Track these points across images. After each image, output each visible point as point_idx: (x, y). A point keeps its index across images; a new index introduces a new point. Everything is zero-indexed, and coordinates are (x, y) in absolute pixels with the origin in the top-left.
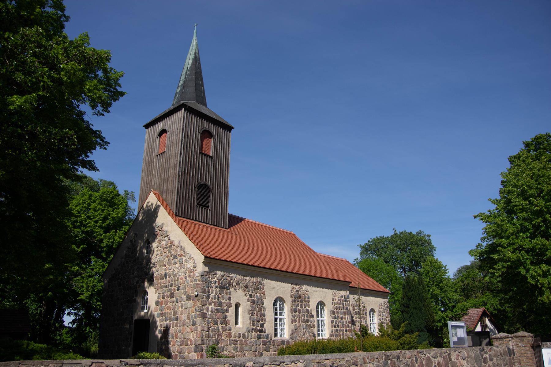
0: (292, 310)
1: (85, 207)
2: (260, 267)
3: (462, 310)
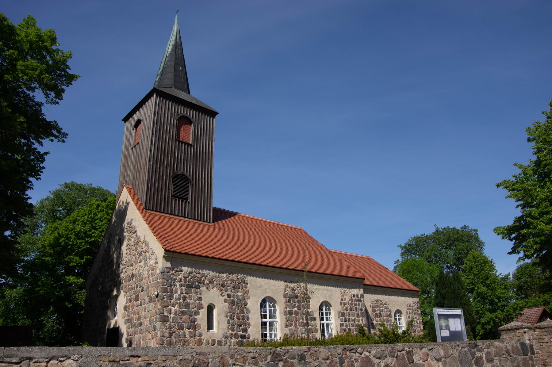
1: (91, 217)
2: (241, 262)
3: (515, 310)
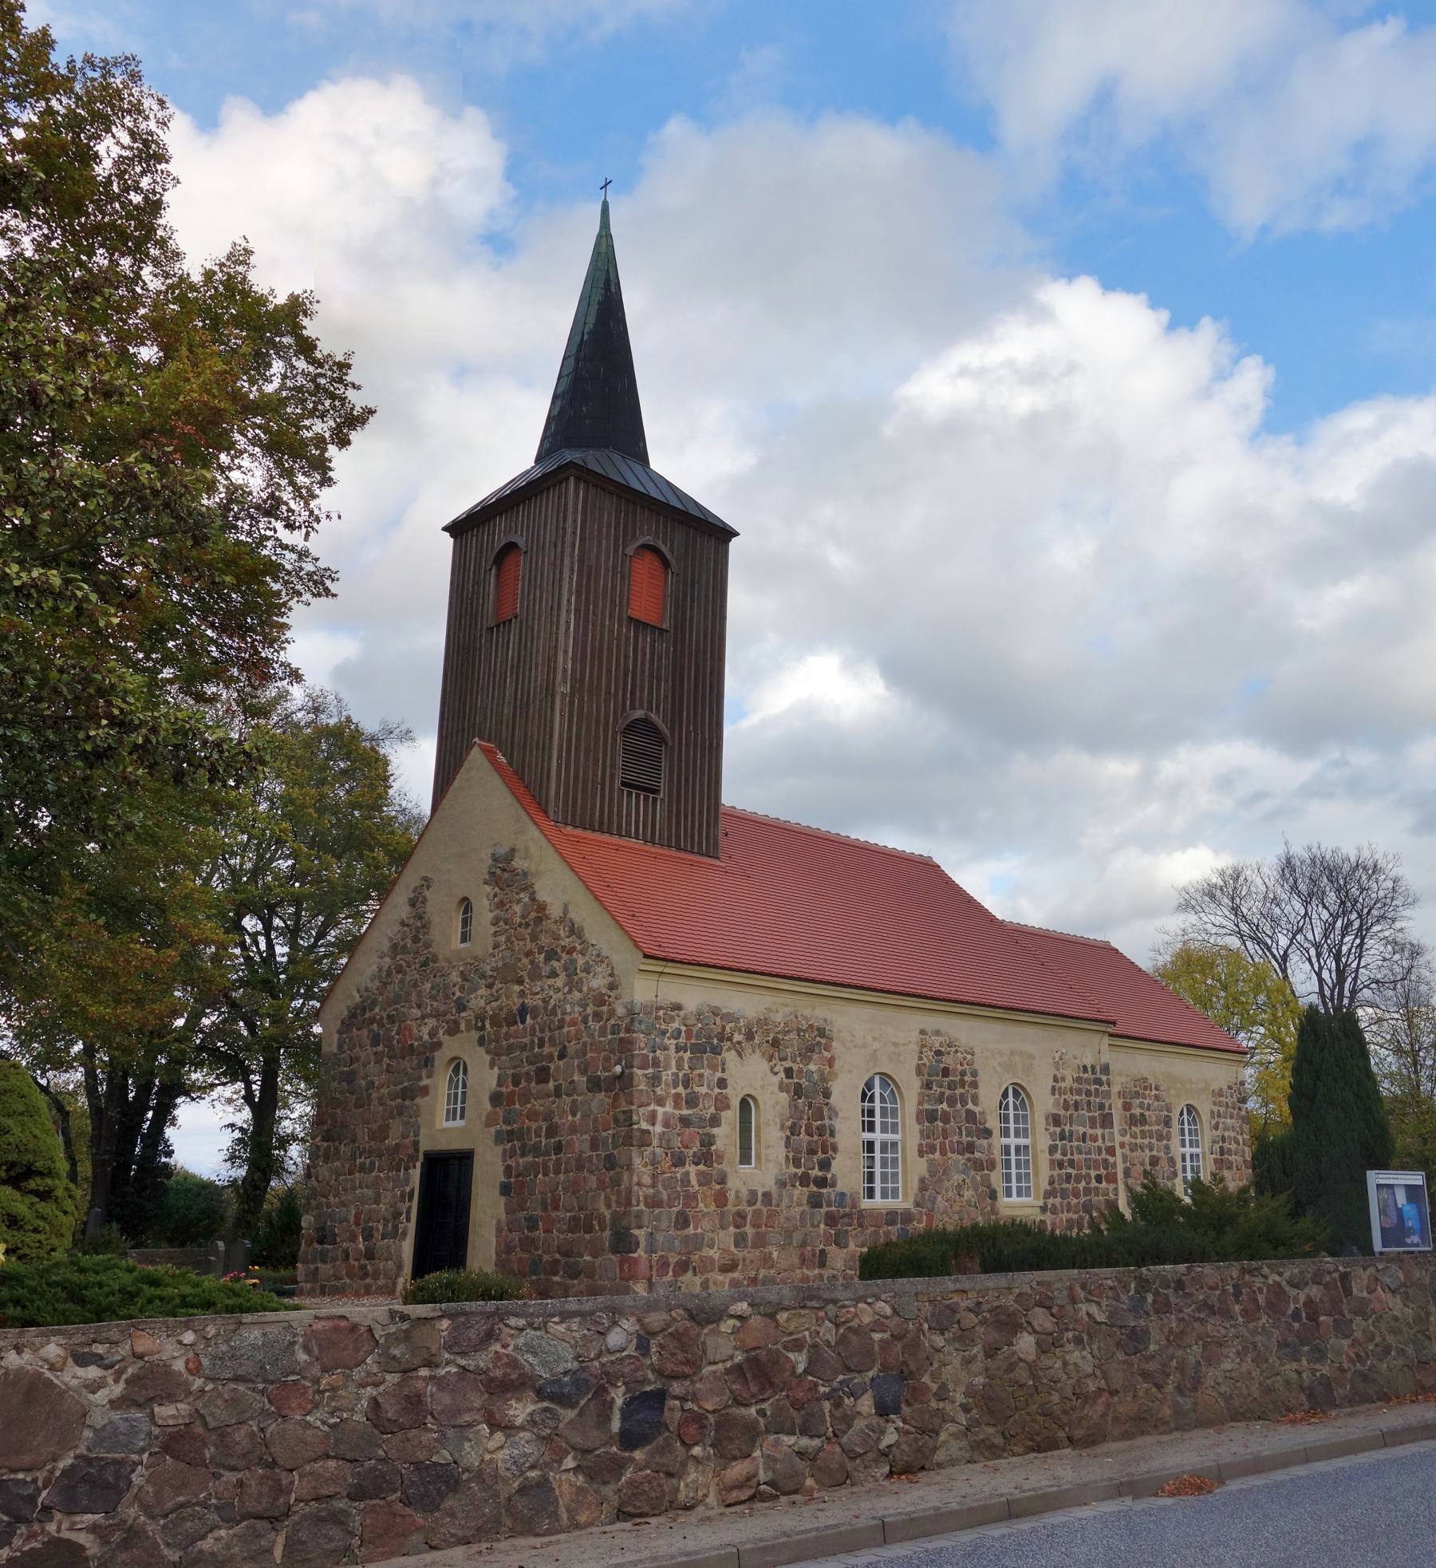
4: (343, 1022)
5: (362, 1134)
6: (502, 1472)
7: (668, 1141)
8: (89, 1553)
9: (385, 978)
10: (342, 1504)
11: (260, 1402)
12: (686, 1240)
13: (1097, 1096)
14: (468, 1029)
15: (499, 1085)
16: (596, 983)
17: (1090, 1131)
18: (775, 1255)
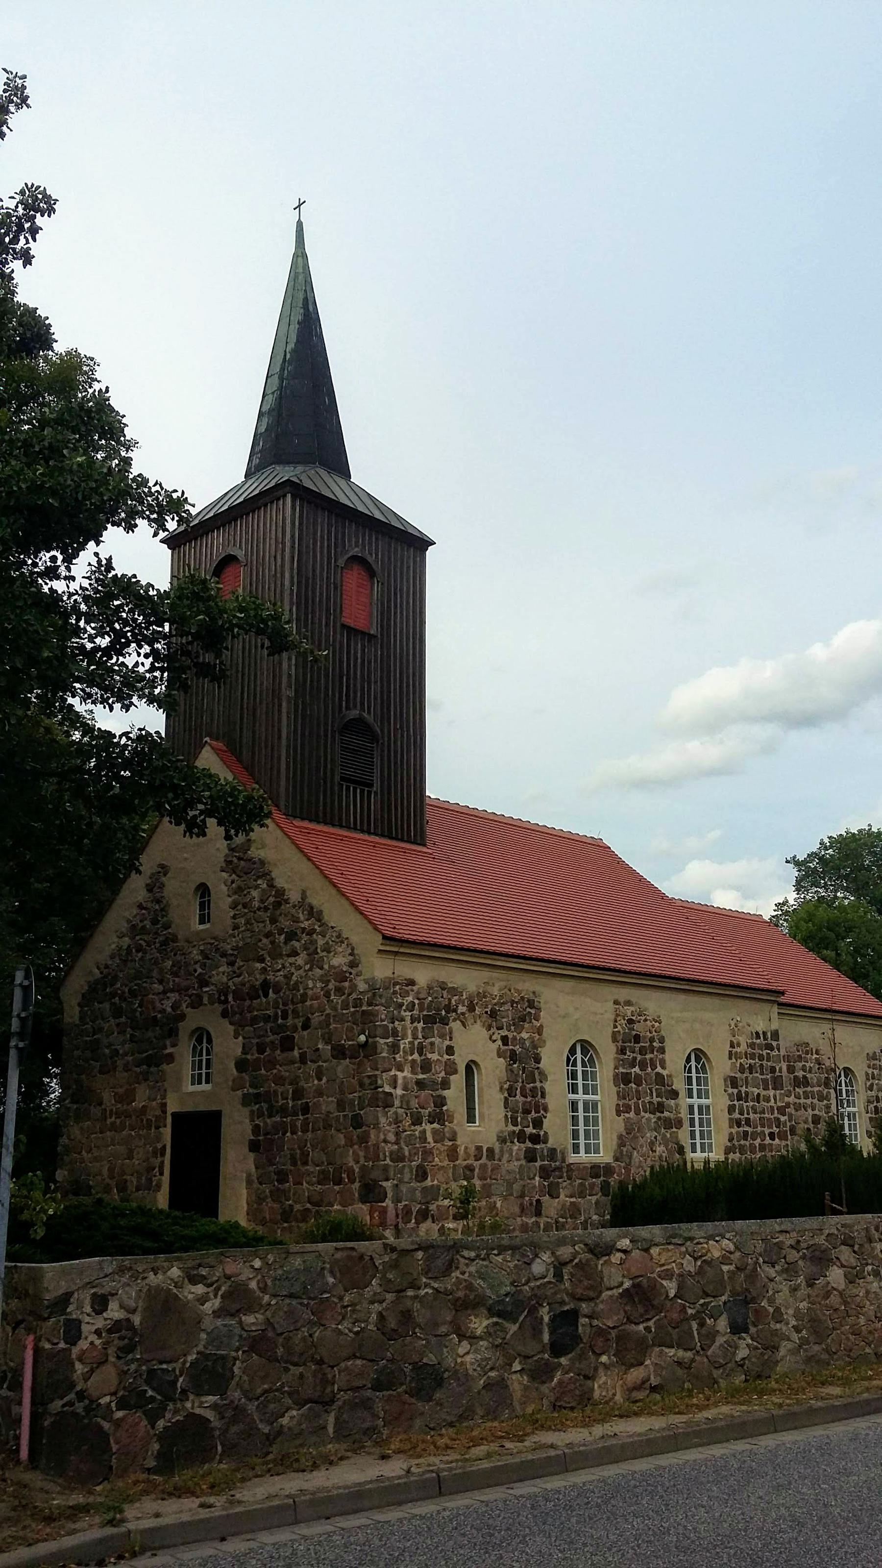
0: (616, 1076)
4: (83, 995)
5: (107, 1097)
6: (470, 1372)
7: (408, 1102)
8: (212, 1425)
9: (124, 956)
10: (369, 1393)
11: (307, 1315)
12: (425, 1190)
13: (768, 1060)
14: (212, 1003)
15: (244, 1052)
16: (336, 961)
17: (763, 1093)
18: (499, 1205)
